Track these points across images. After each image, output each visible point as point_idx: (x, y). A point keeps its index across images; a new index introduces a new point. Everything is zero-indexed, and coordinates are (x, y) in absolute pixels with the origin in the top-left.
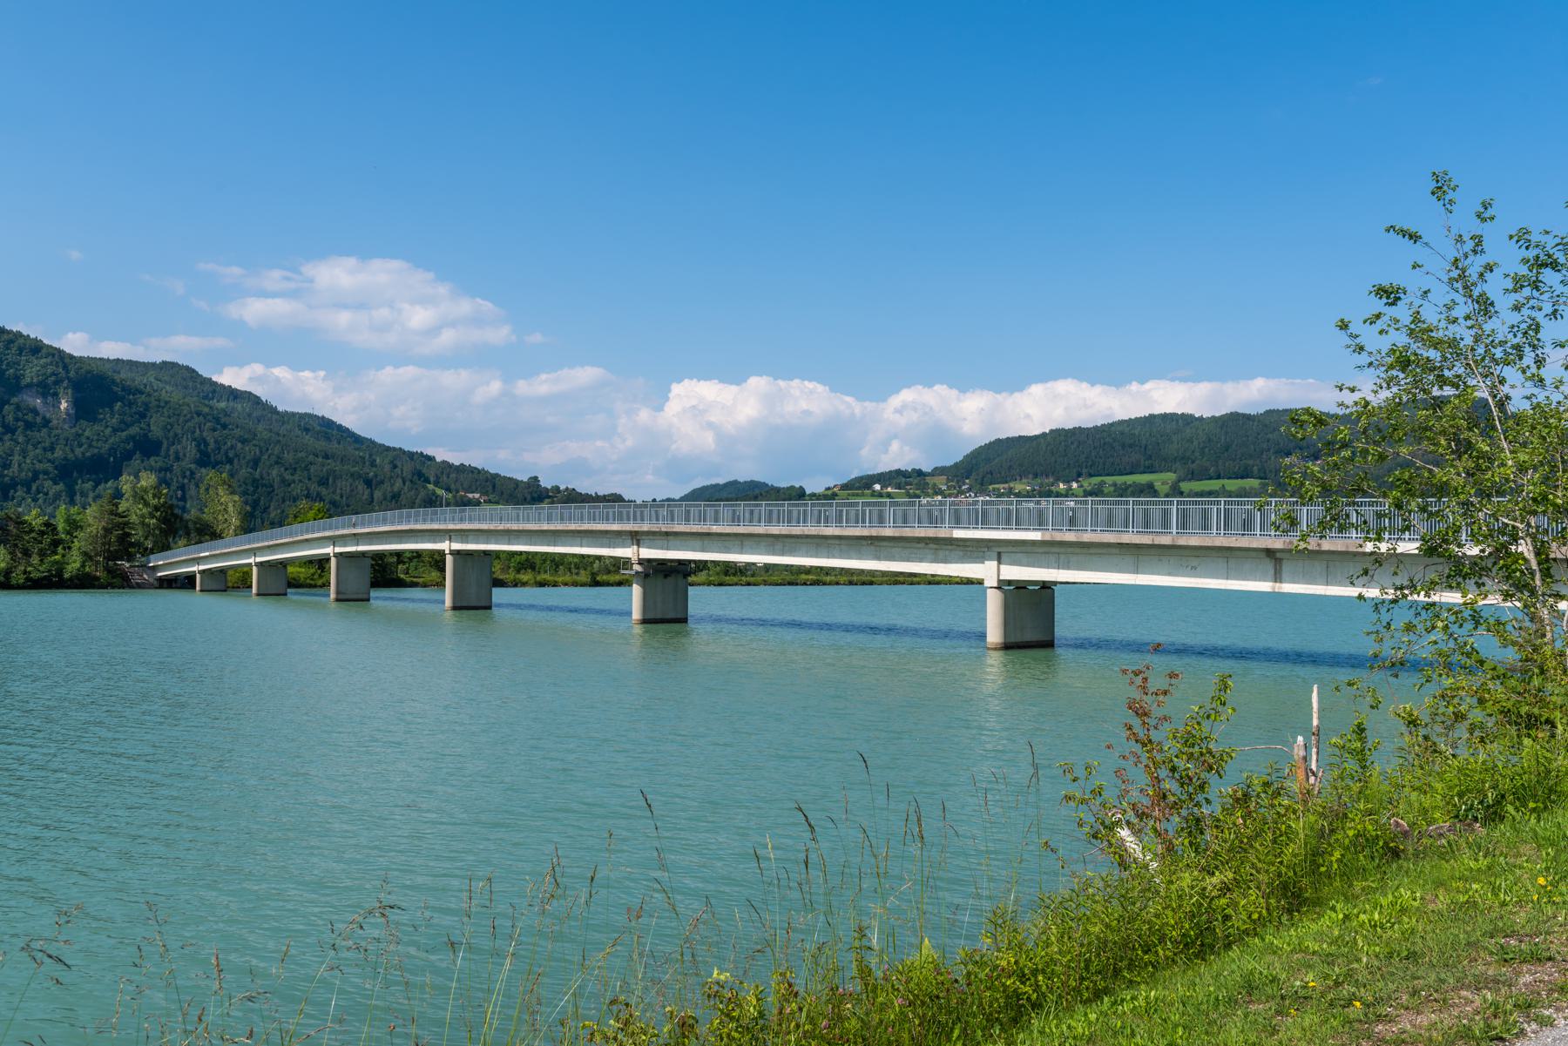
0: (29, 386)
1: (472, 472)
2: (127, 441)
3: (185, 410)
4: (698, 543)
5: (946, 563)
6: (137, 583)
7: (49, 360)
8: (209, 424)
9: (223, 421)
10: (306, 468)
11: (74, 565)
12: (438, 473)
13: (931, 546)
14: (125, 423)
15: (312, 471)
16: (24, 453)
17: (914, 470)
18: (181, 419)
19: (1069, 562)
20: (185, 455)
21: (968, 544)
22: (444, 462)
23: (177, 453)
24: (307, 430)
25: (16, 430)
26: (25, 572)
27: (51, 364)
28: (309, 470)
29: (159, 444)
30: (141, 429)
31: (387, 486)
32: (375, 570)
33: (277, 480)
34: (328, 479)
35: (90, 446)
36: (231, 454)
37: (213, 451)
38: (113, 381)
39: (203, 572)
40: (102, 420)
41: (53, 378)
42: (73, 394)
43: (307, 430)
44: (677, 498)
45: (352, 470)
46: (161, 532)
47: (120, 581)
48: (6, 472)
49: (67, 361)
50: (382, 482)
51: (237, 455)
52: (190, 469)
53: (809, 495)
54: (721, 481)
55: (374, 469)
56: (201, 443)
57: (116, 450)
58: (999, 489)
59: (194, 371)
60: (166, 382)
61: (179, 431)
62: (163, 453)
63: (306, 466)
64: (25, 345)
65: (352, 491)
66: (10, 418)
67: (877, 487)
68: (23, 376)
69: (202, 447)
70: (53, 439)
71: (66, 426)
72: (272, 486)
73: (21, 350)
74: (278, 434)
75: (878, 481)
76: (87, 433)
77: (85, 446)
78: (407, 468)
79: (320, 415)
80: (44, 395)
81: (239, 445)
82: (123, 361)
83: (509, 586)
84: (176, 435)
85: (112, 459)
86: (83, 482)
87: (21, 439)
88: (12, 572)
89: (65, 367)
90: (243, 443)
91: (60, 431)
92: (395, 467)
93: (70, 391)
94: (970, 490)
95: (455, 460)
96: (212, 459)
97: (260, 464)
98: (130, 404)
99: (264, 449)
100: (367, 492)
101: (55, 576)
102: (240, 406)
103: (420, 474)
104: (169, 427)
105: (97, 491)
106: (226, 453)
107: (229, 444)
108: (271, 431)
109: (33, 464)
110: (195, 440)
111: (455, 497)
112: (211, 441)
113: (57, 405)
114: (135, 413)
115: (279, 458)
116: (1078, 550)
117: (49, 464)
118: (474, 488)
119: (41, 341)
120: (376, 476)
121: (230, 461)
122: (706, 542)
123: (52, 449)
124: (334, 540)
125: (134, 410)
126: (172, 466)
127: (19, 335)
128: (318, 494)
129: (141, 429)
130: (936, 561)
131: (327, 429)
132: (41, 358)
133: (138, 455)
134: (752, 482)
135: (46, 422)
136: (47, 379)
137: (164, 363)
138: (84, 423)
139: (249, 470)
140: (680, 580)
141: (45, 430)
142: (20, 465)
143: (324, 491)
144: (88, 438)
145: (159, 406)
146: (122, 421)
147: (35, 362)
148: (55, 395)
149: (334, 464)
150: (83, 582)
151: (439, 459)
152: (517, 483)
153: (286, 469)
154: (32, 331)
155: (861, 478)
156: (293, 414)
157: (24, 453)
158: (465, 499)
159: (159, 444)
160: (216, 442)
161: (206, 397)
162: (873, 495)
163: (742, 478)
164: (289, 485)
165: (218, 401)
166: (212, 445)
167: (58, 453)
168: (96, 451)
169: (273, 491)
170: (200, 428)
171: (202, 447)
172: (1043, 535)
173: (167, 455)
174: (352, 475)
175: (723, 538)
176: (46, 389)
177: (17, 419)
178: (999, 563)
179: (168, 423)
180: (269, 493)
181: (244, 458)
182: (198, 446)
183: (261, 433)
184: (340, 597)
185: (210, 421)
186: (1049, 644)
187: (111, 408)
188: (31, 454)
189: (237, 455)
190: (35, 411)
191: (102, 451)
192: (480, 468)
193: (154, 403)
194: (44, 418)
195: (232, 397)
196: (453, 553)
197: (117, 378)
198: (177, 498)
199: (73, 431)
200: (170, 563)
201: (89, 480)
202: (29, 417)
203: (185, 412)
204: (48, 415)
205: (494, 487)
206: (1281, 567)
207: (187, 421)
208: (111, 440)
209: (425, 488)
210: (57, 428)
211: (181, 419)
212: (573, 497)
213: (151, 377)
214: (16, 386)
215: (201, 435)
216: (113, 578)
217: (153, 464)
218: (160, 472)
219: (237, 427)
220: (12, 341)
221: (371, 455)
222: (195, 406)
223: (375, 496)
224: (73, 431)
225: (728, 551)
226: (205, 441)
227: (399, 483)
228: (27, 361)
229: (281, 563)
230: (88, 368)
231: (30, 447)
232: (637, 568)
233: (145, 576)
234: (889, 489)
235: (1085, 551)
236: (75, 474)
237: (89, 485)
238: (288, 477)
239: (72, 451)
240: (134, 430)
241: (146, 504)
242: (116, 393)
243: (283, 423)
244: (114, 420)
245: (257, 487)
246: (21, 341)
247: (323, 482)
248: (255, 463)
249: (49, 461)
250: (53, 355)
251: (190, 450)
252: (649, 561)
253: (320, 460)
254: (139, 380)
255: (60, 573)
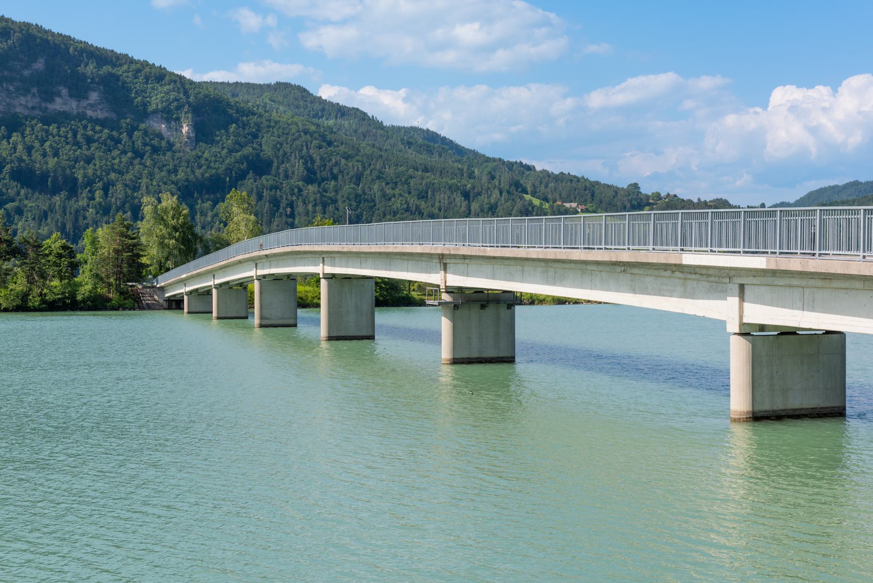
0: (155, 112)
2: (240, 161)
3: (294, 129)
4: (487, 268)
6: (147, 304)
7: (171, 86)
9: (328, 138)
10: (406, 182)
11: (86, 287)
14: (239, 144)
15: (412, 184)
16: (151, 175)
18: (290, 138)
20: (293, 173)
21: (711, 272)
22: (544, 171)
23: (286, 171)
24: (410, 144)
26: (41, 295)
29: (269, 164)
30: (254, 149)
31: (484, 198)
32: (381, 288)
33: (378, 194)
34: (427, 193)
35: (209, 167)
36: (335, 171)
37: (319, 167)
38: (228, 104)
39: (190, 293)
40: (218, 142)
41: (175, 104)
43: (410, 144)
44: (792, 201)
46: (180, 252)
48: (136, 194)
49: (187, 86)
50: (479, 194)
51: (340, 171)
54: (841, 181)
55: (472, 181)
56: (308, 160)
57: (231, 170)
59: (305, 90)
60: (280, 103)
61: (288, 150)
62: (273, 172)
63: (406, 180)
64: (150, 73)
65: (450, 203)
66: (139, 143)
68: (150, 103)
69: (309, 164)
70: (176, 162)
71: (188, 149)
72: (373, 201)
73: (147, 78)
74: (381, 150)
76: (206, 155)
77: (204, 167)
78: (505, 178)
79: (425, 128)
80: (168, 120)
81: (343, 161)
82: (241, 84)
84: (285, 153)
85: (228, 179)
86: (203, 202)
87: (148, 163)
88: (29, 295)
89: (186, 93)
90: (347, 159)
91: (181, 154)
92: (493, 178)
93: (190, 115)
95: (555, 169)
96: (318, 176)
97: (363, 180)
98: (244, 125)
99: (367, 165)
100: (465, 203)
101: (67, 298)
102: (347, 123)
103: (517, 185)
104: (278, 146)
105: (215, 210)
106: (331, 169)
107: (334, 160)
108: (373, 146)
109: (159, 186)
110: (302, 157)
111: (552, 207)
112: (317, 159)
113: (178, 130)
114: (248, 134)
115: (380, 172)
116: (819, 283)
117: (172, 186)
118: (572, 197)
119: (165, 69)
120: (473, 188)
121: (335, 178)
122: (495, 266)
123: (175, 171)
125: (246, 131)
126: (282, 184)
127: (145, 64)
128: (417, 207)
129: (254, 149)
133: (251, 175)
135: (170, 146)
136: (170, 104)
137: (278, 84)
139: (353, 186)
140: (503, 311)
142: (147, 187)
143: (423, 204)
144: (207, 160)
145: (269, 127)
146: (237, 143)
147: (160, 89)
148: (178, 119)
149: (433, 177)
152: (616, 191)
153: (387, 184)
157: (151, 175)
158: (562, 209)
159: (269, 164)
160: (322, 159)
161: (316, 116)
164: (390, 199)
165: (327, 119)
166: (318, 162)
167: (181, 175)
168: (214, 171)
169: (375, 205)
170: (307, 146)
171: (309, 164)
172: (768, 262)
173: (277, 175)
174: (450, 188)
175: (506, 262)
176: (169, 115)
178: (742, 299)
179: (278, 142)
180: (371, 208)
181: (348, 173)
182: (305, 163)
183: (364, 148)
184: (265, 322)
185: (316, 139)
186: (838, 413)
187: (227, 130)
188: (157, 177)
189: (340, 171)
190: (160, 136)
191: (220, 171)
192: (579, 176)
193: (265, 124)
194: (168, 142)
195: (339, 115)
197: (232, 100)
198: (286, 215)
199: (194, 153)
201: (208, 200)
202: (155, 142)
205: (593, 195)
207: (295, 140)
208: (227, 162)
209: (522, 198)
210: (180, 152)
211: (290, 138)
212: (673, 203)
213: (266, 98)
215: (308, 153)
216: (125, 299)
217: (265, 182)
218: (271, 190)
219: (342, 144)
220: (139, 71)
221: (470, 166)
222: (303, 125)
223: (472, 208)
224: (194, 153)
225: (510, 278)
228: (153, 89)
230: (206, 92)
233: (156, 297)
235: (826, 283)
237: (208, 204)
238: (389, 191)
239: (193, 172)
240: (248, 150)
241: (166, 225)
242: (231, 115)
243: (388, 137)
244: (229, 142)
245: (360, 202)
246: (147, 69)
247: (423, 196)
248: (358, 178)
249: (173, 182)
250: (175, 82)
251: (298, 167)
252: (461, 290)
253: (420, 173)
254: (252, 101)
255: (73, 296)
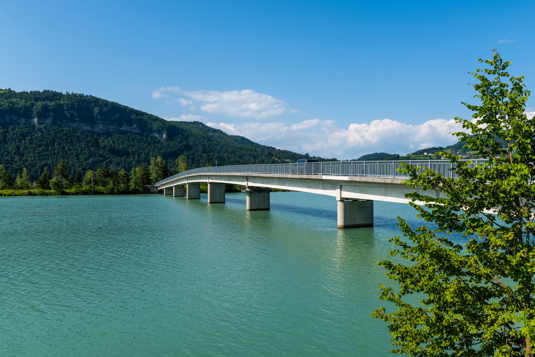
0: (155, 130)
1: (287, 153)
3: (199, 136)
4: (261, 180)
5: (326, 190)
6: (152, 192)
8: (206, 140)
10: (235, 153)
11: (132, 186)
12: (277, 153)
13: (321, 182)
16: (153, 151)
17: (439, 147)
19: (363, 190)
20: (199, 150)
22: (279, 150)
23: (197, 149)
25: (151, 144)
26: (118, 189)
27: (161, 124)
28: (236, 154)
29: (191, 147)
31: (260, 158)
32: (227, 187)
34: (242, 156)
35: (172, 148)
36: (213, 149)
37: (207, 148)
38: (178, 128)
40: (175, 140)
41: (161, 128)
42: (167, 132)
43: (236, 141)
45: (249, 153)
47: (147, 191)
49: (165, 122)
50: (258, 157)
52: (200, 154)
53: (401, 157)
54: (372, 153)
56: (204, 146)
58: (471, 153)
59: (203, 124)
62: (193, 150)
65: (249, 160)
67: (425, 154)
71: (165, 142)
73: (152, 120)
74: (227, 143)
75: (426, 152)
78: (266, 151)
81: (215, 146)
82: (182, 122)
83: (273, 192)
84: (196, 144)
87: (152, 147)
89: (165, 124)
91: (163, 144)
93: (166, 132)
94: (460, 154)
101: (126, 190)
106: (211, 149)
110: (202, 145)
111: (281, 161)
112: (207, 145)
114: (185, 138)
115: (227, 150)
116: (365, 185)
120: (256, 155)
123: (161, 149)
124: (187, 178)
127: (152, 115)
128: (239, 161)
129: (186, 142)
130: (323, 189)
131: (243, 140)
132: (158, 122)
133: (185, 151)
134: (382, 153)
135: (160, 141)
137: (194, 122)
138: (170, 141)
139: (218, 154)
140: (266, 194)
141: (159, 144)
142: (152, 155)
144: (171, 146)
145: (191, 135)
146: (181, 140)
147: (156, 123)
148: (162, 133)
150: (136, 192)
151: (277, 149)
153: (229, 153)
154: (155, 114)
155: (420, 151)
156: (233, 136)
157: (153, 151)
159: (191, 147)
160: (208, 146)
161: (206, 132)
162: (424, 157)
163: (379, 152)
164: (230, 158)
167: (163, 151)
172: (349, 178)
173: (194, 150)
174: (249, 155)
176: (159, 132)
177: (151, 141)
179: (194, 140)
180: (224, 161)
182: (203, 147)
184: (190, 198)
188: (155, 151)
190: (156, 138)
191: (175, 149)
192: (290, 151)
193: (190, 134)
194: (159, 140)
196: (210, 183)
199: (167, 144)
200: (163, 185)
202: (155, 140)
203: (199, 137)
204: (160, 139)
205: (294, 157)
206: (439, 194)
207: (200, 139)
208: (178, 146)
209: (272, 158)
214: (151, 131)
216: (145, 190)
217: (190, 153)
219: (215, 141)
220: (150, 117)
222: (202, 135)
223: (256, 161)
224: (167, 144)
226: (205, 145)
227: (263, 157)
229: (182, 186)
231: (155, 149)
232: (248, 189)
233: (155, 190)
234: (430, 154)
236: (168, 157)
237: (172, 160)
238: (230, 156)
239: (167, 150)
240: (184, 143)
241: (158, 167)
246: (152, 117)
247: (240, 157)
248: (220, 152)
249: (160, 153)
250: (161, 121)
251: (201, 148)
252: (252, 187)
253: (239, 150)
254: (186, 127)
255: (128, 189)
